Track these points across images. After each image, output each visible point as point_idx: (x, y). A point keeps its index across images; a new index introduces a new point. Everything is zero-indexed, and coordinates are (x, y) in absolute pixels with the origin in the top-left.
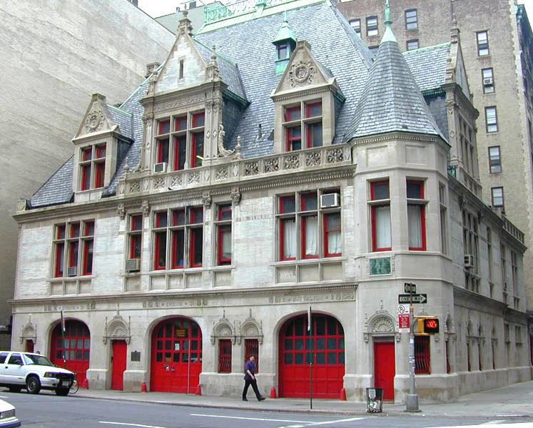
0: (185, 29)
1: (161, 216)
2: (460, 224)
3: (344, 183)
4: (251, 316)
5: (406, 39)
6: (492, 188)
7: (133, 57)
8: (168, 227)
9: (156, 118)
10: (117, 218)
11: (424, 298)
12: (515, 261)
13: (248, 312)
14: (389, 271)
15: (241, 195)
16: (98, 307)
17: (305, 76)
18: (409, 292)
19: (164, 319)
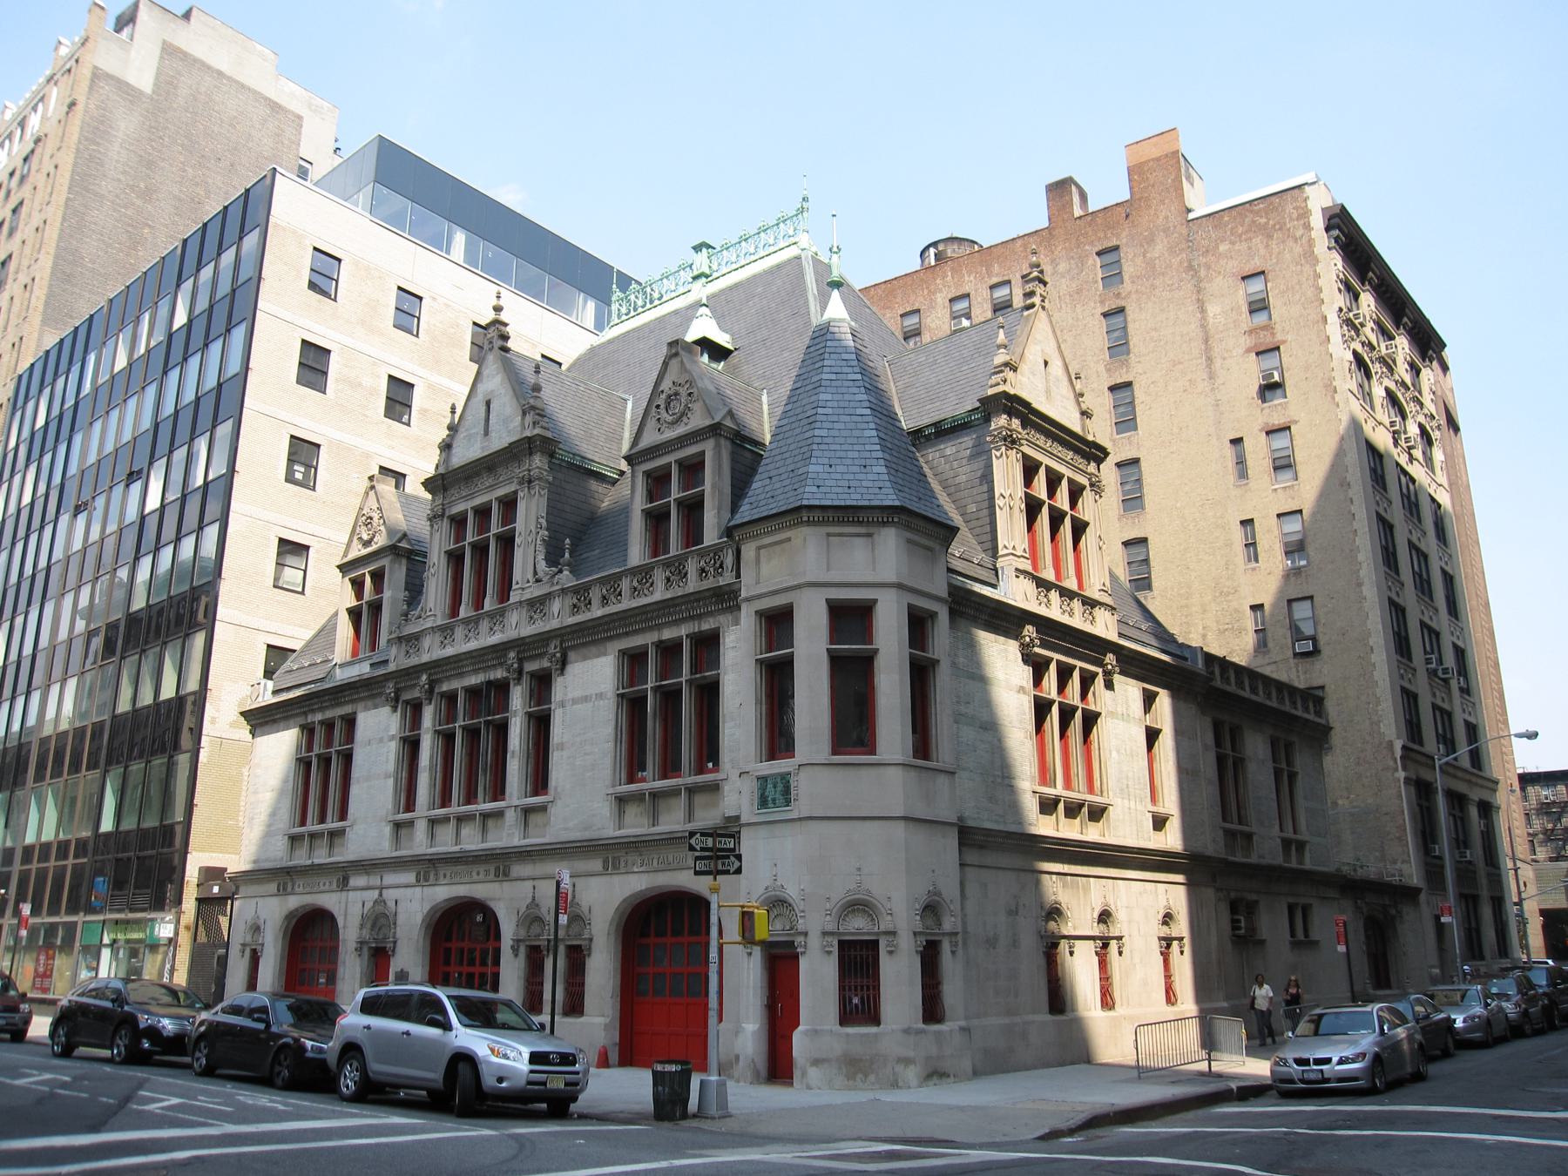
1: (451, 698)
3: (722, 620)
6: (1290, 602)
16: (356, 881)
18: (702, 849)
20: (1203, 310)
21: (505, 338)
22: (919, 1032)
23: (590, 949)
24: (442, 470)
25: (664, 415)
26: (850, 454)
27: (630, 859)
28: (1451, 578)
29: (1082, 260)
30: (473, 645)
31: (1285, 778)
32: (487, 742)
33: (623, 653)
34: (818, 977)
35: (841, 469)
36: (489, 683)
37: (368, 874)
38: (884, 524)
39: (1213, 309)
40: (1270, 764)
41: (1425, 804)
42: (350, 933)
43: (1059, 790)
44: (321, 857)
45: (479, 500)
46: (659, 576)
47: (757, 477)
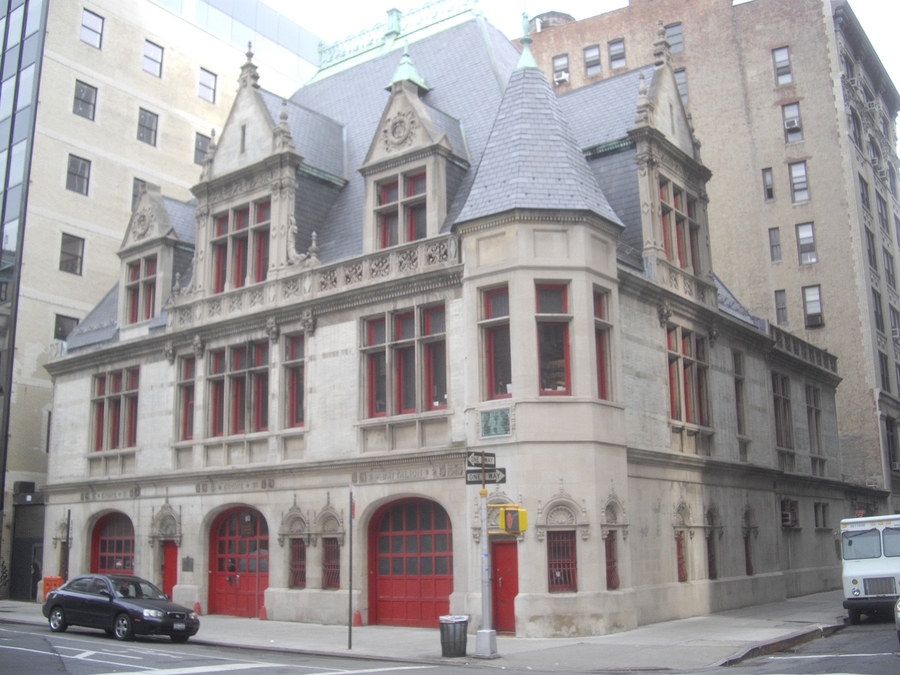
0: (248, 79)
1: (219, 355)
3: (450, 293)
8: (227, 373)
9: (211, 213)
10: (165, 364)
11: (502, 476)
12: (816, 402)
13: (325, 497)
14: (507, 430)
16: (145, 492)
18: (476, 465)
20: (743, 73)
21: (256, 77)
22: (606, 596)
23: (180, 543)
24: (206, 179)
25: (391, 138)
26: (548, 170)
30: (237, 313)
31: (814, 413)
33: (363, 319)
34: (532, 559)
35: (542, 181)
36: (251, 343)
38: (576, 223)
39: (751, 73)
40: (805, 405)
41: (891, 434)
42: (143, 529)
44: (115, 473)
45: (239, 202)
46: (393, 260)
47: (474, 186)
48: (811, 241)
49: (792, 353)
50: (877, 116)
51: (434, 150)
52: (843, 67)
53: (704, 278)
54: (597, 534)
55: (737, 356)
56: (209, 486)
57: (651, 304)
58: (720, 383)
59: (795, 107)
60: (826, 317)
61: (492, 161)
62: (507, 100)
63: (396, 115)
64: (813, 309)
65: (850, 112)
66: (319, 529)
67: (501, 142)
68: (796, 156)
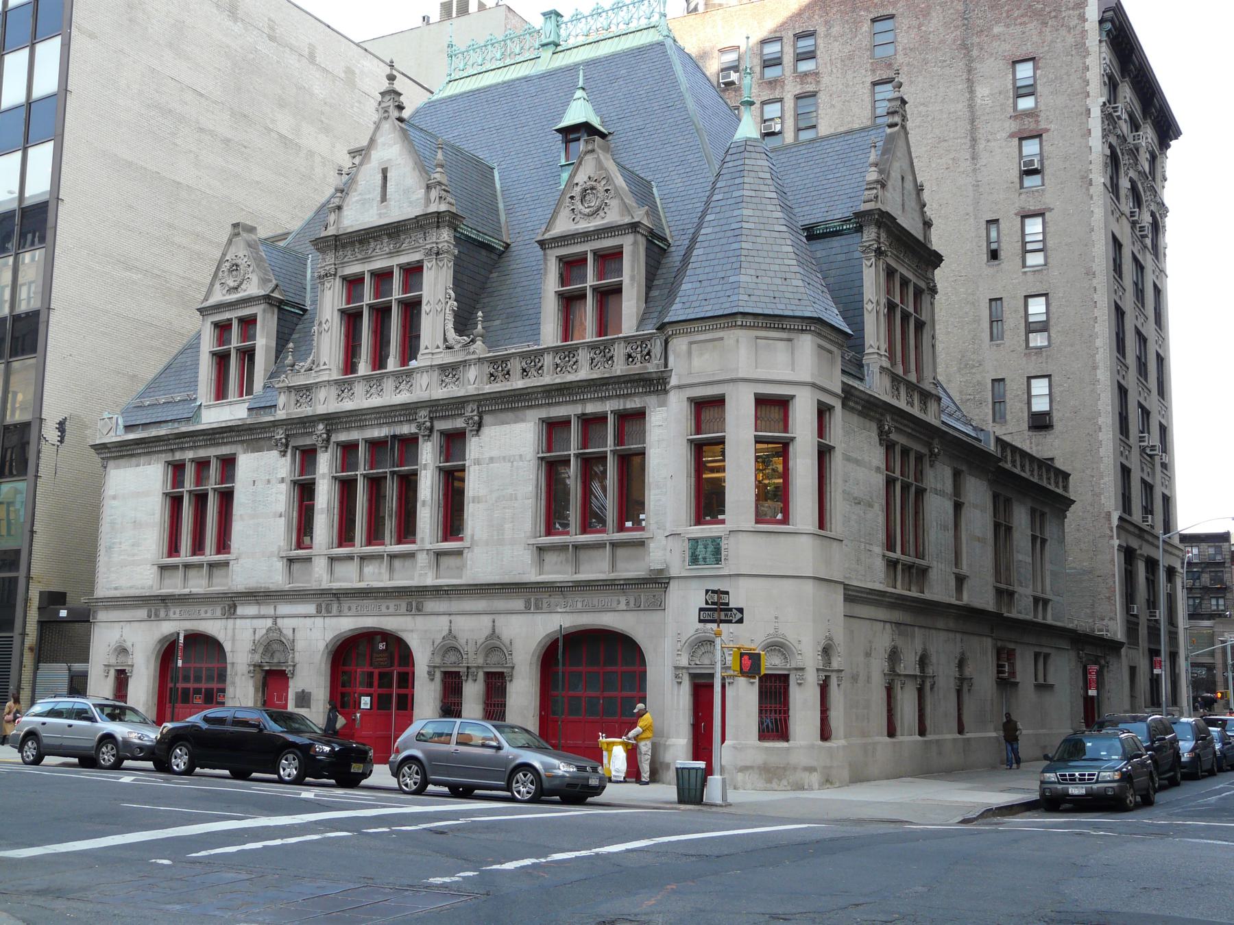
0: (391, 109)
1: (349, 449)
2: (878, 469)
3: (650, 402)
4: (494, 631)
5: (870, 79)
7: (326, 130)
8: (361, 471)
9: (339, 274)
10: (275, 453)
11: (739, 616)
13: (491, 624)
14: (718, 561)
15: (481, 418)
16: (240, 610)
17: (594, 203)
18: (713, 603)
19: (350, 634)
20: (971, 91)
26: (772, 267)
27: (553, 600)
28: (1162, 359)
29: (857, 23)
30: (376, 401)
31: (1039, 542)
32: (391, 491)
33: (543, 420)
36: (394, 437)
37: (258, 603)
39: (982, 91)
43: (897, 555)
48: (1044, 318)
49: (1017, 471)
50: (1142, 151)
51: (634, 227)
52: (1105, 91)
53: (927, 386)
54: (812, 679)
55: (957, 475)
56: (335, 607)
57: (871, 419)
58: (937, 508)
59: (1037, 141)
60: (1056, 416)
61: (708, 250)
62: (725, 177)
63: (586, 179)
64: (1040, 405)
65: (1108, 152)
66: (480, 661)
67: (717, 229)
68: (1033, 206)
